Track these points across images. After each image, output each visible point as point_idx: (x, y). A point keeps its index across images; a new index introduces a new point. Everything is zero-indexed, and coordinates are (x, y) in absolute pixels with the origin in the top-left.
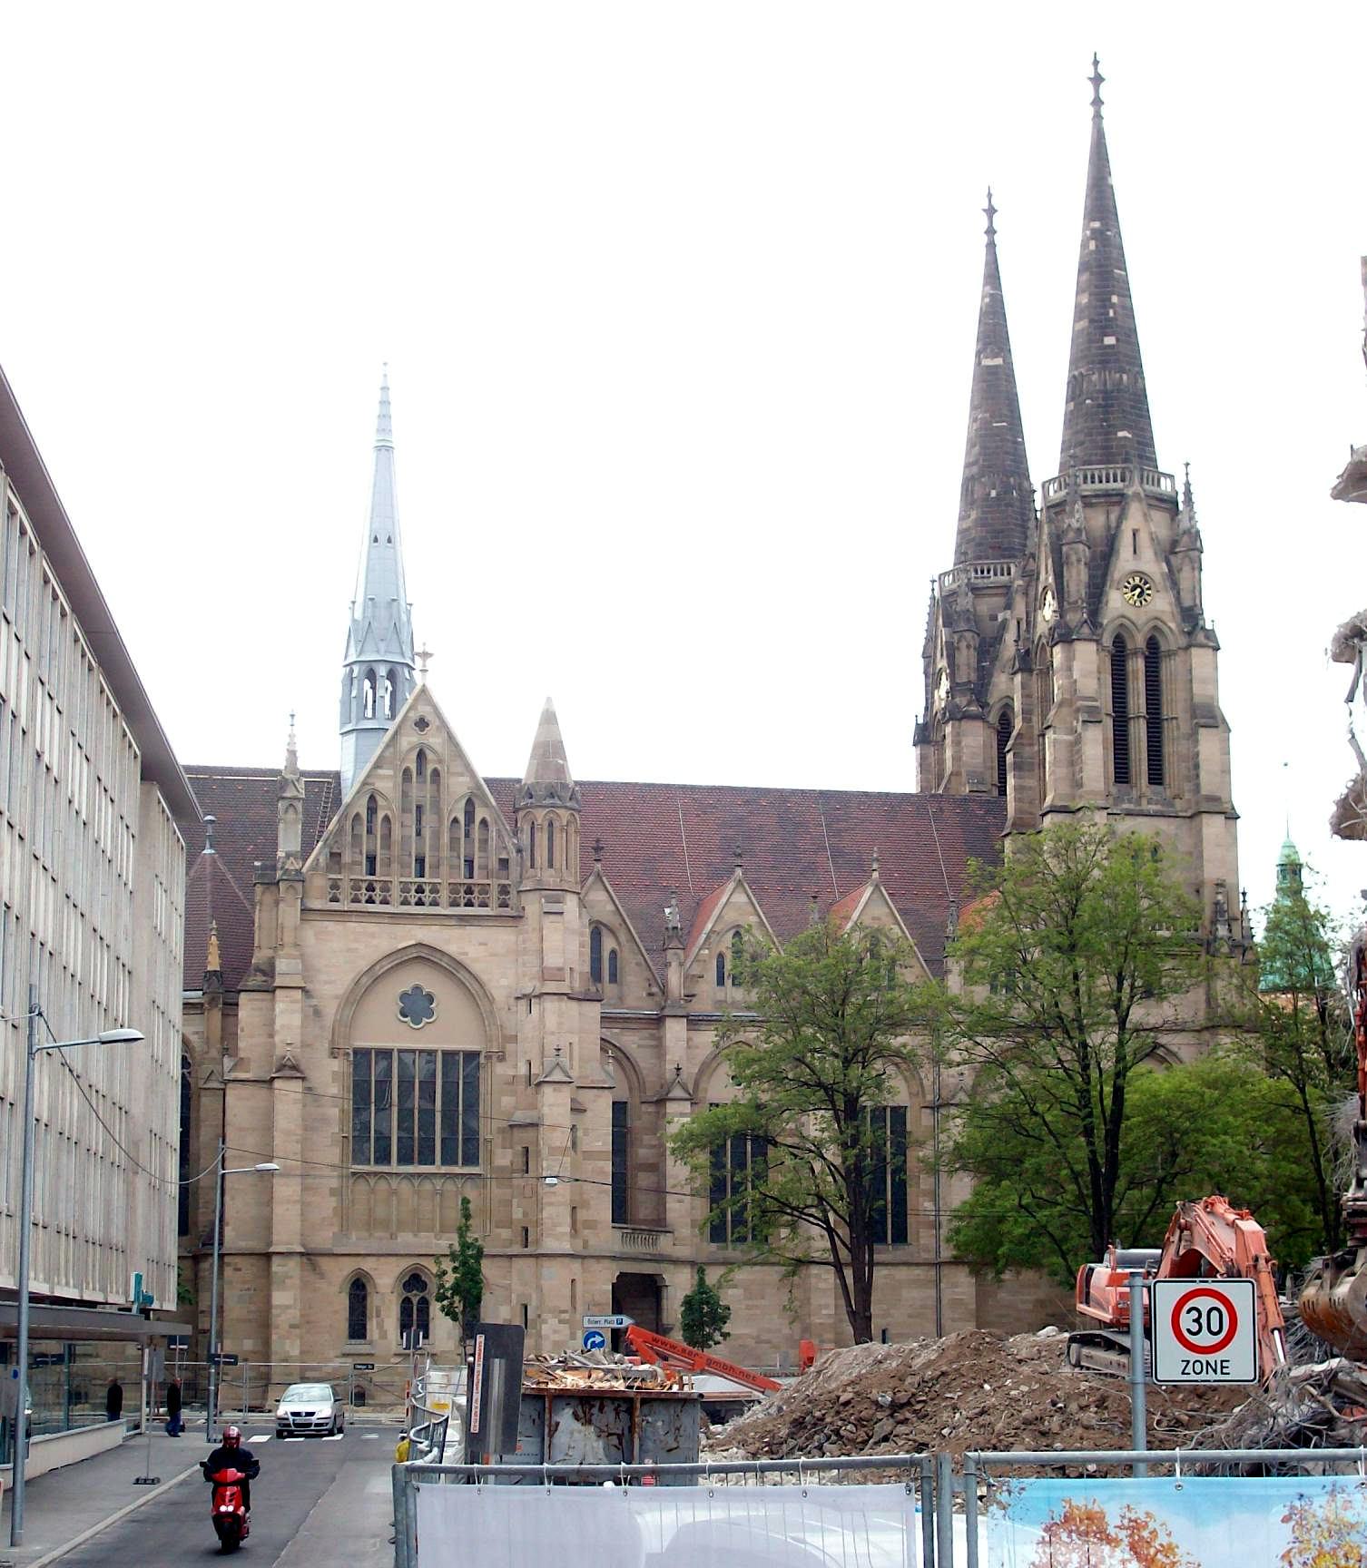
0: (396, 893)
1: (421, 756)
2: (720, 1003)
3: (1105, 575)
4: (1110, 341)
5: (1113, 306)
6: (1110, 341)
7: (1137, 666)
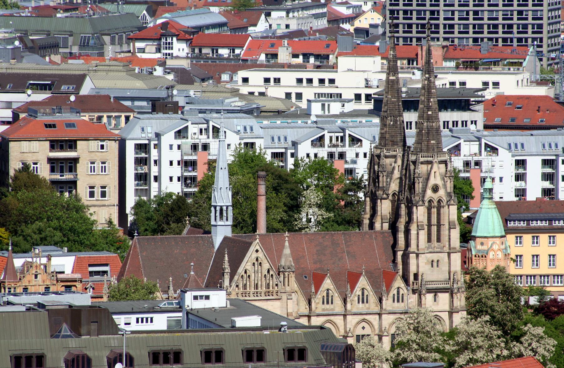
0: (251, 294)
1: (257, 260)
2: (323, 310)
3: (426, 185)
4: (430, 113)
5: (431, 102)
6: (430, 113)
7: (434, 211)
